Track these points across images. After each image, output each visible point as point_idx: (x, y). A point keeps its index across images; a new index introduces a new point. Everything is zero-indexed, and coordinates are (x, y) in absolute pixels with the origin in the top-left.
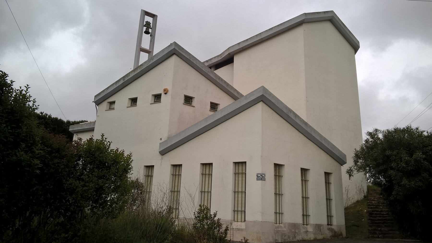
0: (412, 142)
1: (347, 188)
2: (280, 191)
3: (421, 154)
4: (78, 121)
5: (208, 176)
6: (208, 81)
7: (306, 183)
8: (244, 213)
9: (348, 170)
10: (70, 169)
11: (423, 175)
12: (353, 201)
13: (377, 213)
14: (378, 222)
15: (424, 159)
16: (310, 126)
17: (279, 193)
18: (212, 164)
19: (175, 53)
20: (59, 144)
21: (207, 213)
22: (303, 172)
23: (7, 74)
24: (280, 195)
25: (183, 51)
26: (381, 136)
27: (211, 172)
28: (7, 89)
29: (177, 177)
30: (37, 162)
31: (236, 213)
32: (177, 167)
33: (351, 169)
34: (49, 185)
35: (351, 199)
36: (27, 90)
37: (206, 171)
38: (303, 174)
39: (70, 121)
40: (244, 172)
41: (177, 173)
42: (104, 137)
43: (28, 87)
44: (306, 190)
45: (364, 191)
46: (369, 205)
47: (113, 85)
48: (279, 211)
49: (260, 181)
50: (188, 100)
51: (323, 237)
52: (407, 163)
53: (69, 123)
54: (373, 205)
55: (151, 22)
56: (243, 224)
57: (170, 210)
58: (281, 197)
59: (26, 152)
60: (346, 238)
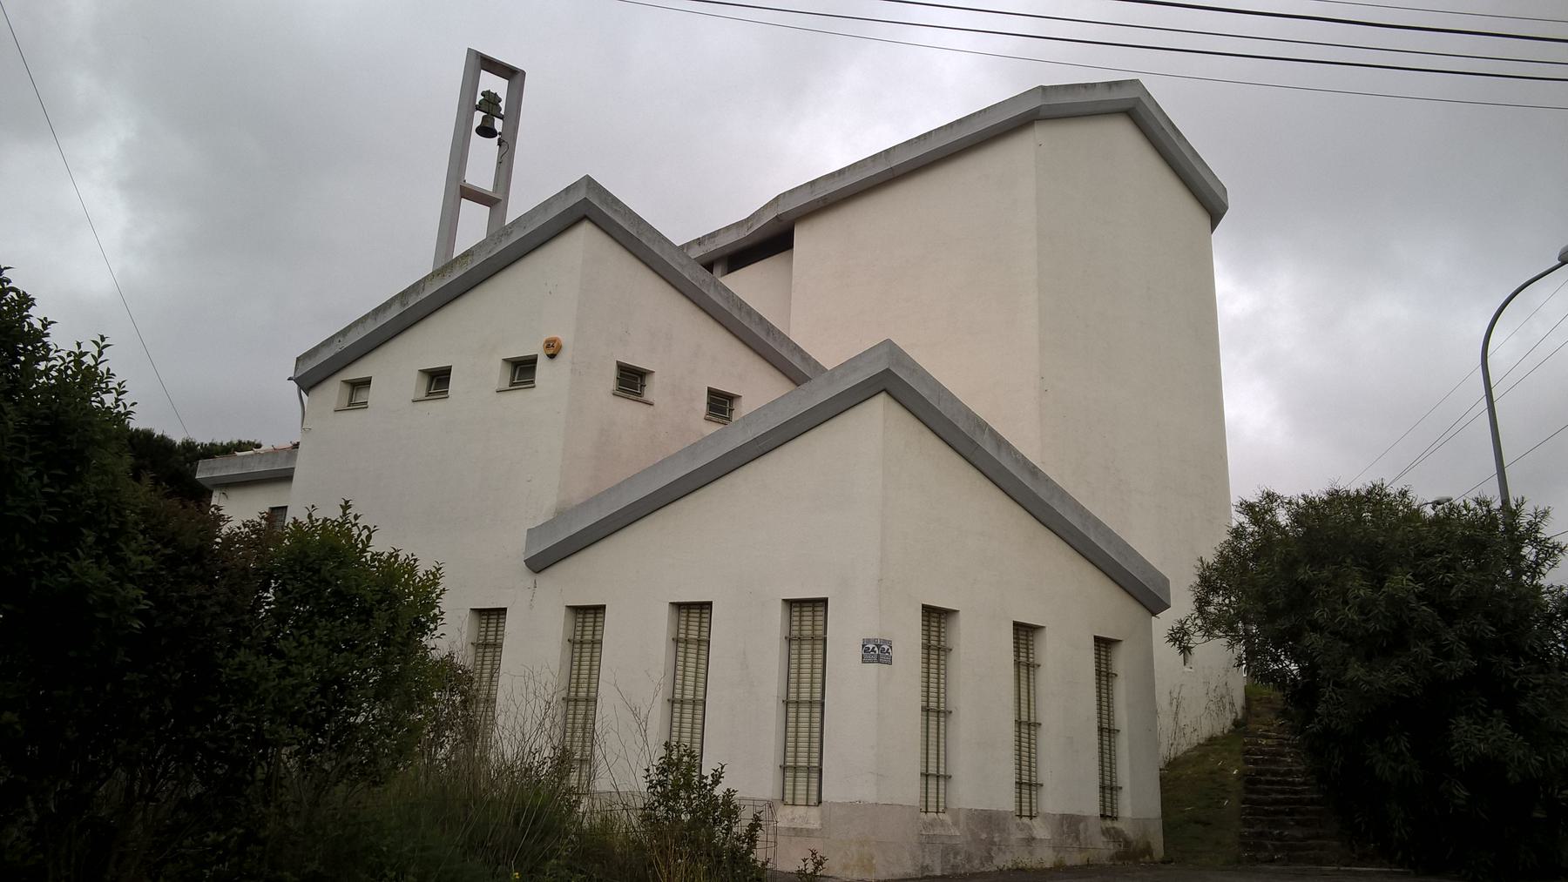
0: (1382, 538)
1: (1175, 695)
2: (942, 700)
3: (1410, 577)
4: (225, 443)
5: (695, 647)
6: (703, 316)
7: (1031, 673)
8: (816, 775)
9: (1173, 630)
10: (238, 619)
11: (1415, 650)
12: (1196, 738)
13: (1274, 778)
14: (1272, 809)
15: (1421, 597)
16: (1048, 480)
17: (938, 707)
18: (710, 604)
19: (587, 213)
20: (201, 533)
21: (690, 767)
22: (1021, 637)
23: (33, 299)
24: (942, 715)
25: (616, 210)
26: (1283, 517)
27: (706, 634)
28: (30, 348)
29: (587, 649)
30: (133, 591)
31: (789, 774)
32: (588, 616)
33: (1182, 628)
34: (172, 670)
35: (1188, 730)
36: (100, 353)
37: (687, 629)
38: (1021, 641)
39: (194, 443)
40: (819, 633)
41: (588, 637)
42: (352, 512)
43: (104, 344)
44: (1032, 699)
45: (1232, 704)
46: (1248, 752)
47: (362, 322)
48: (938, 767)
49: (873, 667)
50: (631, 380)
51: (1085, 860)
52: (1363, 608)
53: (194, 453)
54: (1263, 753)
55: (503, 95)
56: (814, 812)
57: (564, 761)
58: (945, 722)
59: (98, 560)
60: (1163, 862)
